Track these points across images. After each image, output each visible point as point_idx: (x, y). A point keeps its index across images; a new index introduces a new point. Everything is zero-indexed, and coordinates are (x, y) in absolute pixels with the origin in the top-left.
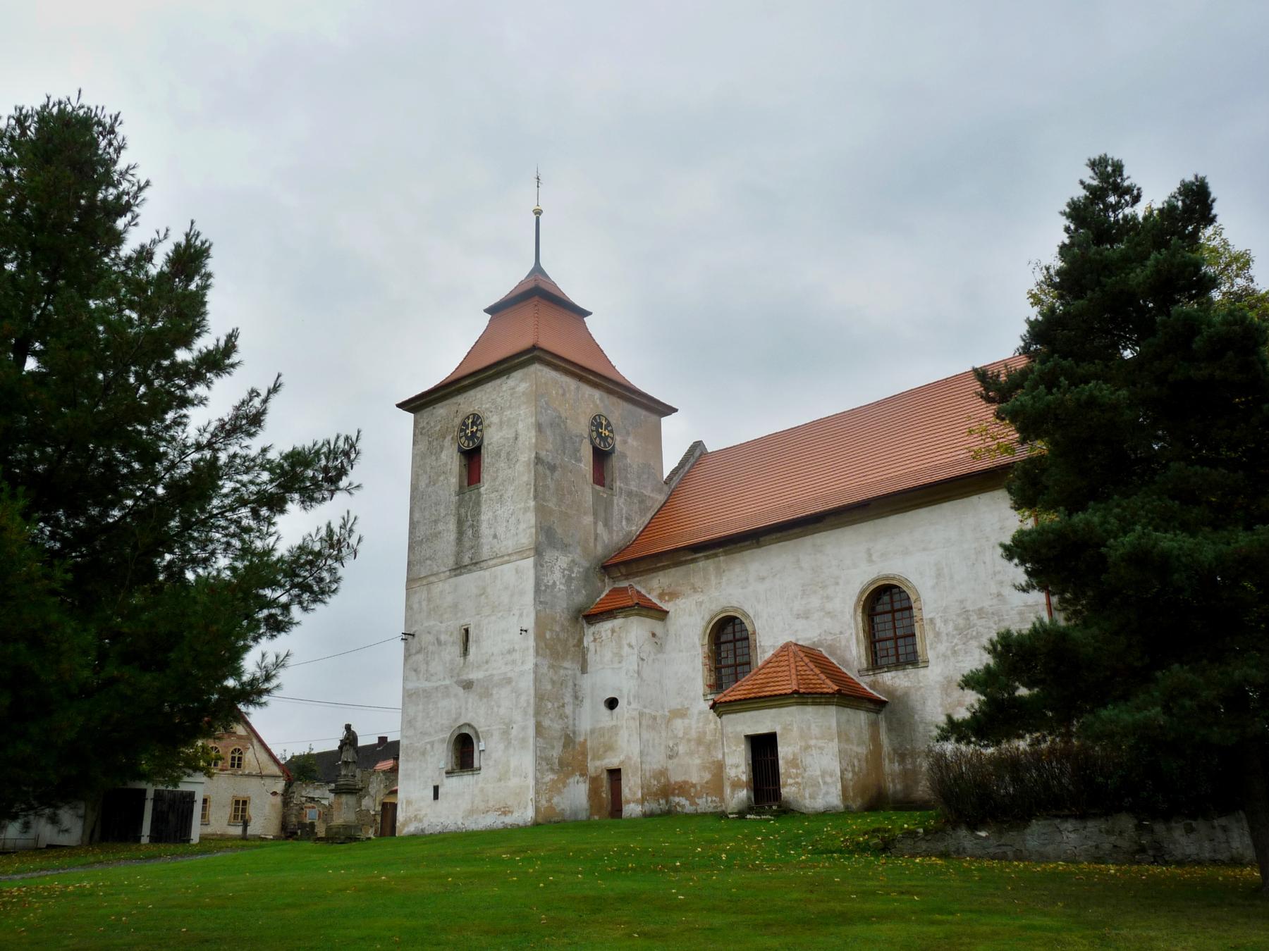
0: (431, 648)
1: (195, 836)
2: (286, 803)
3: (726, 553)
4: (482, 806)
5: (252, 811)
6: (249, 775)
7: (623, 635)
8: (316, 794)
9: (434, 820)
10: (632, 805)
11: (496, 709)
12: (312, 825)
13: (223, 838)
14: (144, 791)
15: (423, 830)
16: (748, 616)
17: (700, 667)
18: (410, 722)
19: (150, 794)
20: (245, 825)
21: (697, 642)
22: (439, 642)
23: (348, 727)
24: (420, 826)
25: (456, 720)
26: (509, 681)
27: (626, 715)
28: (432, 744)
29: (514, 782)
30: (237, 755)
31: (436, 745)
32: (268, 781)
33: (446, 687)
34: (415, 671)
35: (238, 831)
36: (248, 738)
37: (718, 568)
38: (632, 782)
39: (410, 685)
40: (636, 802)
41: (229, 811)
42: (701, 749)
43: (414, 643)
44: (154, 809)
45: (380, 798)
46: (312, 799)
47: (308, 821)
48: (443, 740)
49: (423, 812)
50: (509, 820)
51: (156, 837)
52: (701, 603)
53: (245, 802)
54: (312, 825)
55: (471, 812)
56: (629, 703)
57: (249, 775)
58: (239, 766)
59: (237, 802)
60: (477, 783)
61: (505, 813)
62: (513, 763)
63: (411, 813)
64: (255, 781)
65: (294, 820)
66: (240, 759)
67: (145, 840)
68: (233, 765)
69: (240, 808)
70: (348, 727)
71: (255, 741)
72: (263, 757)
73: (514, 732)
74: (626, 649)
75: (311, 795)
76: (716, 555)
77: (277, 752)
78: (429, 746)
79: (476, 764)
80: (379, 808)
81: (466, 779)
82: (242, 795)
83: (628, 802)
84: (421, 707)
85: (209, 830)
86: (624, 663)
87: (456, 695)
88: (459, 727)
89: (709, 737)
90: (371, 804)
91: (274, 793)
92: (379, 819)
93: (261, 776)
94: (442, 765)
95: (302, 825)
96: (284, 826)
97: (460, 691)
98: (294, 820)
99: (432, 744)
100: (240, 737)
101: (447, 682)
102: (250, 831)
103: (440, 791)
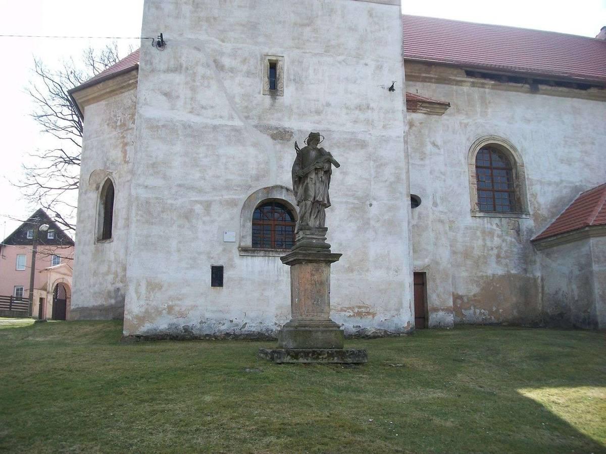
3: (493, 87)
7: (425, 131)
10: (441, 314)
16: (515, 149)
17: (467, 184)
21: (462, 158)
22: (220, 67)
25: (257, 178)
26: (363, 145)
27: (431, 217)
28: (208, 206)
29: (376, 275)
31: (215, 208)
37: (483, 99)
38: (440, 289)
40: (448, 310)
42: (469, 262)
52: (466, 125)
56: (435, 204)
62: (374, 250)
73: (374, 211)
74: (429, 148)
76: (483, 86)
83: (436, 310)
86: (427, 162)
89: (477, 252)
94: (231, 236)
99: (208, 206)
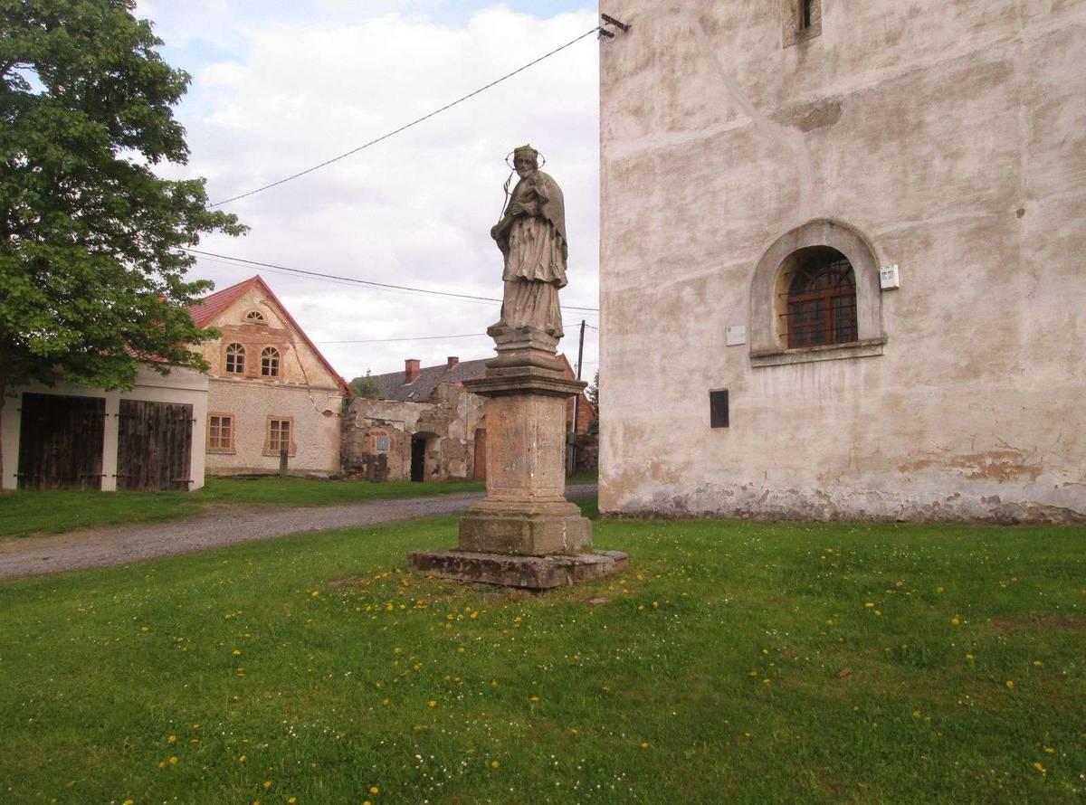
0: (681, 48)
1: (197, 478)
2: (346, 427)
4: (898, 448)
5: (296, 435)
6: (291, 387)
8: (387, 415)
9: (719, 481)
11: (939, 165)
12: (383, 458)
13: (256, 476)
14: (103, 401)
15: (679, 503)
18: (625, 238)
19: (112, 408)
20: (284, 456)
23: (525, 160)
24: (671, 491)
25: (779, 215)
28: (700, 286)
30: (270, 357)
31: (713, 288)
32: (318, 396)
33: (740, 135)
34: (637, 112)
35: (273, 464)
36: (285, 334)
39: (618, 152)
41: (263, 436)
43: (629, 48)
44: (121, 433)
45: (473, 423)
46: (382, 422)
47: (377, 453)
48: (735, 275)
49: (679, 458)
50: (1017, 494)
51: (129, 478)
53: (285, 424)
54: (383, 458)
55: (853, 464)
57: (291, 387)
58: (274, 372)
59: (274, 424)
60: (871, 382)
61: (1000, 473)
63: (641, 455)
64: (299, 395)
65: (357, 451)
66: (275, 363)
67: (109, 484)
68: (265, 372)
69: (280, 428)
70: (525, 160)
71: (296, 339)
72: (310, 361)
75: (379, 417)
77: (341, 372)
78: (688, 293)
79: (866, 327)
80: (471, 437)
81: (829, 376)
82: (281, 415)
84: (657, 197)
85: (223, 462)
87: (774, 152)
88: (796, 232)
90: (461, 431)
91: (328, 413)
92: (472, 450)
93: (308, 388)
94: (739, 334)
95: (368, 458)
96: (344, 458)
97: (793, 138)
98: (357, 451)
100: (274, 332)
101: (742, 121)
102: (292, 464)
103: (733, 406)
